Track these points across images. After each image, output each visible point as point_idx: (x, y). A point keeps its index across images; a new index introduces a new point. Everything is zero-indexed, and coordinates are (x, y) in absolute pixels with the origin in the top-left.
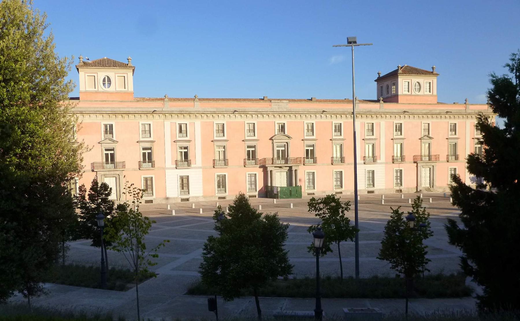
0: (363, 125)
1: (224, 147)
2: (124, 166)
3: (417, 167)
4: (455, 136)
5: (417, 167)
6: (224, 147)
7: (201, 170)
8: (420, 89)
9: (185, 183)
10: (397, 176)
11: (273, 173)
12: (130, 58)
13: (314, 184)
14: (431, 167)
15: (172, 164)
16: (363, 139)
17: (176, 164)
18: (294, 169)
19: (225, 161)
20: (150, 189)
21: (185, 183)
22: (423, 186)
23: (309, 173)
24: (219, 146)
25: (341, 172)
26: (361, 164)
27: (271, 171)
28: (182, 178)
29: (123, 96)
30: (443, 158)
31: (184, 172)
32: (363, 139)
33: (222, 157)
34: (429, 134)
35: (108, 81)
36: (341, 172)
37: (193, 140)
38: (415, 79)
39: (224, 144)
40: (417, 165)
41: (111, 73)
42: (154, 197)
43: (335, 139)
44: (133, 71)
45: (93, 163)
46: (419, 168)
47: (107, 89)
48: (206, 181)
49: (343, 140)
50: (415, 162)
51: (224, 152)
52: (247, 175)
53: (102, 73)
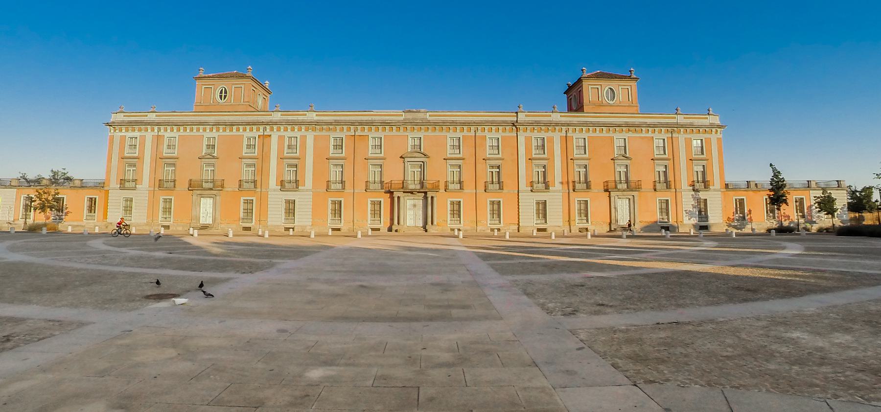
0: (528, 140)
1: (544, 167)
2: (222, 186)
3: (610, 197)
4: (458, 156)
5: (610, 197)
9: (542, 209)
10: (661, 209)
11: (402, 199)
13: (587, 216)
14: (631, 197)
18: (429, 195)
19: (499, 183)
21: (542, 209)
22: (561, 224)
25: (667, 201)
26: (526, 191)
27: (399, 198)
28: (288, 202)
30: (647, 185)
31: (542, 196)
36: (667, 201)
38: (606, 85)
39: (544, 162)
41: (614, 84)
42: (502, 225)
43: (489, 159)
45: (191, 180)
46: (612, 199)
47: (611, 102)
49: (588, 159)
50: (606, 190)
53: (221, 85)
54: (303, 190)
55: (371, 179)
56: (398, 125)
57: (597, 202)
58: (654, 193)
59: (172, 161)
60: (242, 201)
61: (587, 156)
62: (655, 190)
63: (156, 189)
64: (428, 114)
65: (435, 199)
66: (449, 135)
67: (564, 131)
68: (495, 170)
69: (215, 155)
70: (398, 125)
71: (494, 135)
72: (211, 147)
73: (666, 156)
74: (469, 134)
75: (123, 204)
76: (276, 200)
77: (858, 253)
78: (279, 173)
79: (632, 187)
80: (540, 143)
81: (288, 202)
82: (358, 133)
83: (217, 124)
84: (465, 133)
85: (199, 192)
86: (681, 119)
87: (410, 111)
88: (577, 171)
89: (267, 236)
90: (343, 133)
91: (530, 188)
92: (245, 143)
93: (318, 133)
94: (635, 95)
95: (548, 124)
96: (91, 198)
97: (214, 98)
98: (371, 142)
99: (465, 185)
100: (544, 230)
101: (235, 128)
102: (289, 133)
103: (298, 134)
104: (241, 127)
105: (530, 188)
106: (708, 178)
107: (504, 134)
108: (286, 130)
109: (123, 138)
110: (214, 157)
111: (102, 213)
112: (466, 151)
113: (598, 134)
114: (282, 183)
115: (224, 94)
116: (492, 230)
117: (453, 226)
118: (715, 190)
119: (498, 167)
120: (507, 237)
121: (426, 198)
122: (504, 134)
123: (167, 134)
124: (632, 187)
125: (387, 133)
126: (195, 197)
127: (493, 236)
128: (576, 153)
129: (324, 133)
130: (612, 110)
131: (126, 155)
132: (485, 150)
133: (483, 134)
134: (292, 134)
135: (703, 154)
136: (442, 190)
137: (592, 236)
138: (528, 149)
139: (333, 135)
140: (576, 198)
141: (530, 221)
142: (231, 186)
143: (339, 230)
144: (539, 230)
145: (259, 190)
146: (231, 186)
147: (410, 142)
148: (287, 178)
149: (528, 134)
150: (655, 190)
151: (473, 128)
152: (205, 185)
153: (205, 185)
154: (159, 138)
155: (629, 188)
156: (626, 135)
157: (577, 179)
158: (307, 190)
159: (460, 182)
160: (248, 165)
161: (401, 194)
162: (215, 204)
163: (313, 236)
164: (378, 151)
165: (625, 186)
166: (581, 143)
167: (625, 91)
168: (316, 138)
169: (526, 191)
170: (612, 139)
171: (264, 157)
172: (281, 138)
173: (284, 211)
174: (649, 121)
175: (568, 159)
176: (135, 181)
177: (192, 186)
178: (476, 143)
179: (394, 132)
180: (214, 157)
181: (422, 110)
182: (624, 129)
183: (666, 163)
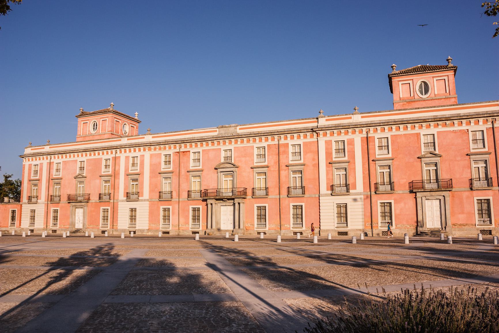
0: (328, 143)
2: (89, 199)
3: (416, 198)
6: (436, 165)
7: (148, 202)
8: (426, 91)
9: (343, 213)
12: (449, 58)
14: (442, 198)
15: (327, 190)
16: (467, 155)
17: (332, 190)
19: (346, 186)
20: (389, 218)
21: (343, 213)
23: (480, 202)
24: (294, 172)
26: (326, 195)
27: (211, 204)
28: (339, 206)
29: (439, 102)
32: (467, 155)
33: (387, 179)
34: (435, 150)
35: (425, 88)
36: (390, 203)
37: (351, 161)
39: (389, 162)
40: (416, 196)
41: (427, 77)
44: (455, 71)
45: (412, 182)
46: (419, 200)
47: (424, 97)
48: (153, 214)
50: (411, 192)
51: (436, 170)
52: (476, 202)
53: (418, 80)
54: (142, 200)
55: (475, 176)
56: (213, 140)
57: (403, 205)
58: (471, 192)
59: (58, 181)
60: (101, 210)
61: (390, 156)
62: (471, 189)
63: (49, 202)
64: (238, 128)
65: (241, 205)
66: (256, 145)
67: (364, 132)
68: (298, 175)
69: (84, 175)
70: (213, 140)
71: (296, 141)
72: (82, 168)
73: (486, 149)
74: (273, 143)
75: (128, 213)
76: (124, 208)
77: (461, 256)
78: (126, 187)
79: (444, 186)
80: (341, 147)
81: (339, 206)
82: (183, 149)
83: (85, 151)
84: (270, 142)
85: (74, 204)
86: (323, 122)
87: (222, 127)
88: (379, 173)
89: (236, 240)
90: (171, 151)
91: (330, 192)
92: (377, 144)
93: (153, 152)
94: (452, 86)
95: (346, 127)
96: (14, 211)
97: (89, 131)
98: (291, 150)
99: (270, 190)
100: (346, 233)
101: (97, 152)
102: (336, 137)
103: (345, 138)
104: (101, 152)
105: (330, 192)
106: (350, 181)
107: (306, 140)
108: (339, 134)
109: (30, 165)
110: (83, 177)
111: (19, 222)
112: (270, 160)
113: (402, 132)
114: (332, 187)
115: (95, 126)
116: (295, 233)
117: (260, 230)
118: (145, 200)
119: (301, 172)
120: (407, 242)
121: (234, 204)
122: (306, 140)
123: (56, 160)
124: (444, 186)
125: (205, 147)
126: (71, 208)
127: (259, 239)
128: (378, 153)
129: (158, 152)
130: (424, 104)
131: (103, 173)
132: (288, 157)
133: (286, 142)
134: (134, 155)
135: (484, 147)
136: (249, 197)
137: (239, 239)
138: (328, 154)
139: (164, 152)
140: (378, 201)
141: (329, 224)
142: (94, 199)
143: (168, 233)
144: (340, 233)
145: (112, 201)
146: (94, 199)
147: (223, 154)
148: (130, 190)
149: (328, 138)
150: (471, 189)
151: (276, 137)
152: (427, 186)
153: (79, 199)
154: (367, 140)
155: (439, 189)
156: (433, 130)
157: (379, 180)
158: (145, 200)
159: (391, 183)
160: (106, 182)
161: (213, 201)
162: (84, 213)
163: (279, 241)
164: (298, 158)
165: (434, 186)
166: (479, 136)
167: (440, 83)
168: (151, 155)
169: (326, 195)
170: (418, 135)
171: (115, 175)
172: (127, 158)
173: (336, 215)
174: (462, 112)
175: (369, 160)
176: (138, 193)
177: (71, 199)
178: (280, 150)
179: (210, 147)
180: (83, 177)
181: (234, 125)
182: (432, 124)
183: (486, 157)
